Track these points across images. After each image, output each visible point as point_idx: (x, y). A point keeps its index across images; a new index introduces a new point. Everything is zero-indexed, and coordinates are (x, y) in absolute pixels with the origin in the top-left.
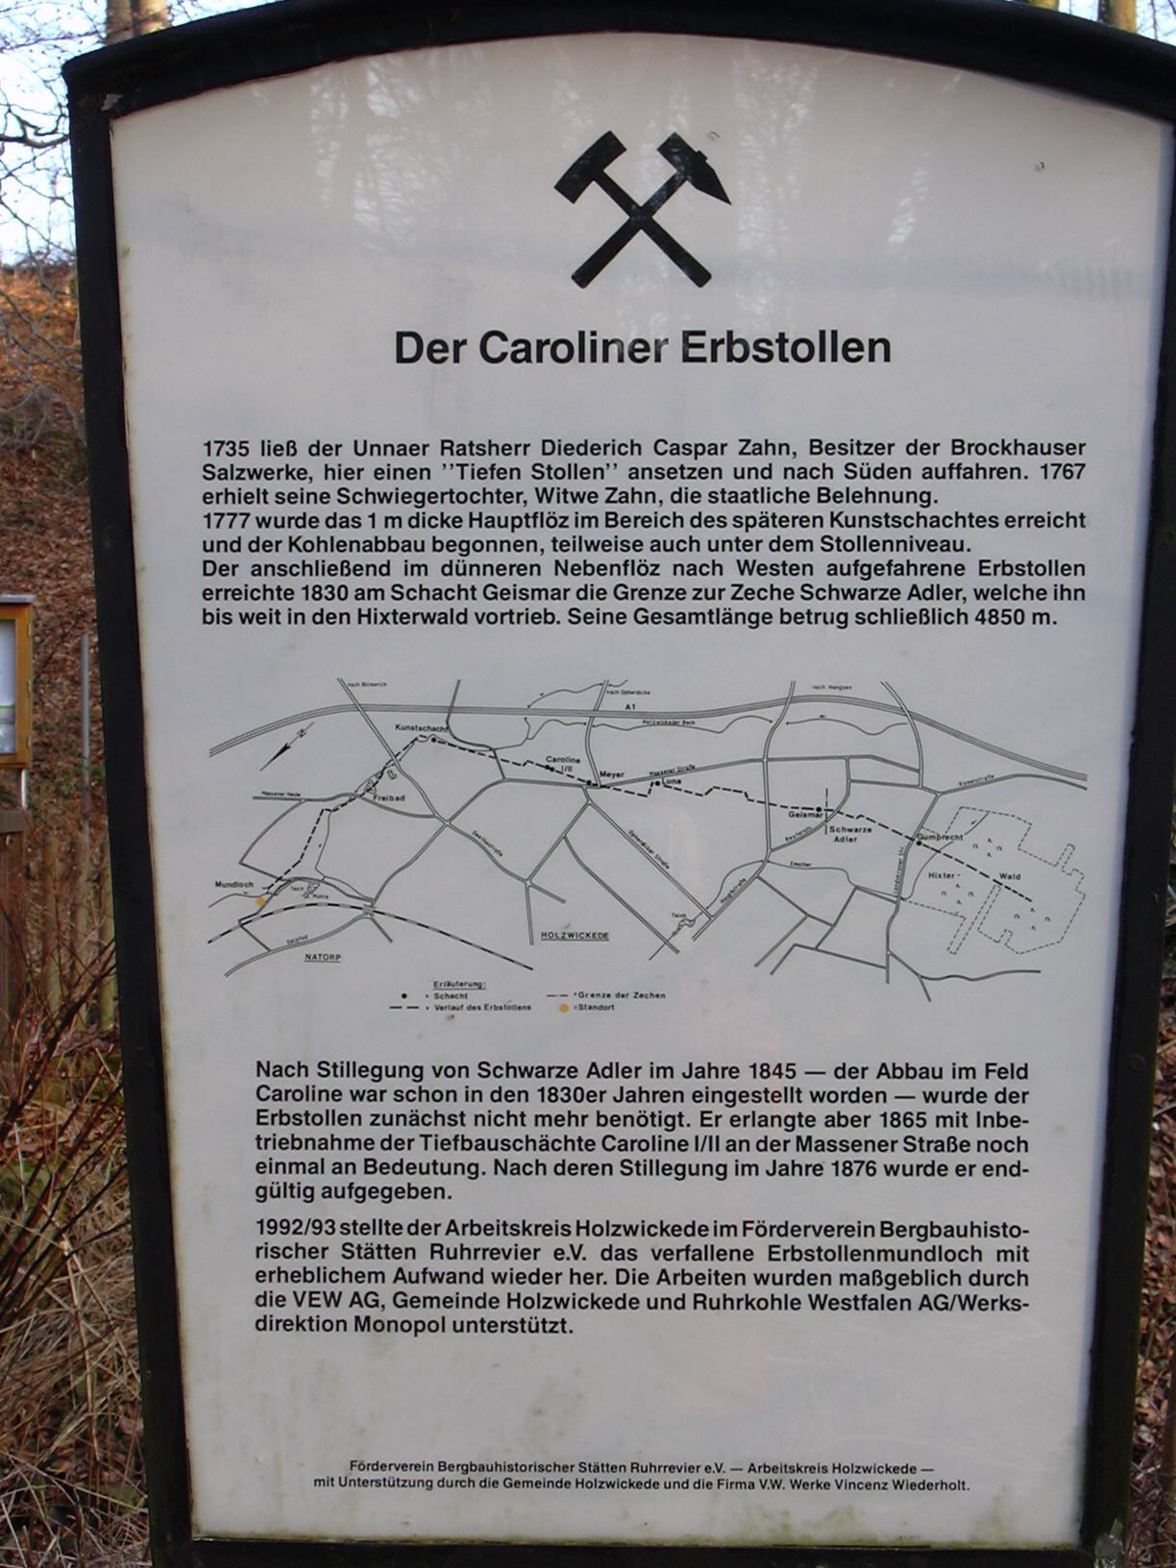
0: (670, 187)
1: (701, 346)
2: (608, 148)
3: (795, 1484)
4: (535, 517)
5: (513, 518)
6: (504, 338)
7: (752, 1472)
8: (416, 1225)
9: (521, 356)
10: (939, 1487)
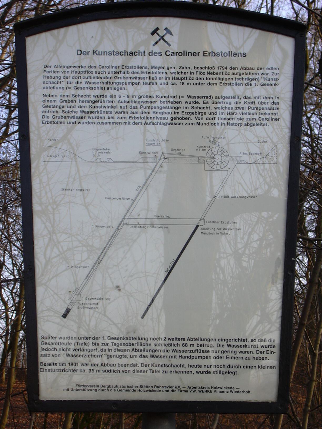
0: (158, 34)
1: (207, 53)
2: (157, 29)
3: (200, 391)
4: (186, 78)
5: (182, 78)
6: (170, 52)
7: (188, 341)
8: (198, 78)
9: (131, 54)
10: (243, 392)
